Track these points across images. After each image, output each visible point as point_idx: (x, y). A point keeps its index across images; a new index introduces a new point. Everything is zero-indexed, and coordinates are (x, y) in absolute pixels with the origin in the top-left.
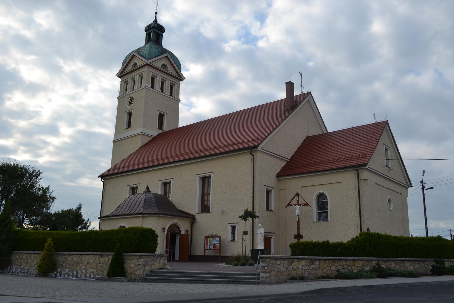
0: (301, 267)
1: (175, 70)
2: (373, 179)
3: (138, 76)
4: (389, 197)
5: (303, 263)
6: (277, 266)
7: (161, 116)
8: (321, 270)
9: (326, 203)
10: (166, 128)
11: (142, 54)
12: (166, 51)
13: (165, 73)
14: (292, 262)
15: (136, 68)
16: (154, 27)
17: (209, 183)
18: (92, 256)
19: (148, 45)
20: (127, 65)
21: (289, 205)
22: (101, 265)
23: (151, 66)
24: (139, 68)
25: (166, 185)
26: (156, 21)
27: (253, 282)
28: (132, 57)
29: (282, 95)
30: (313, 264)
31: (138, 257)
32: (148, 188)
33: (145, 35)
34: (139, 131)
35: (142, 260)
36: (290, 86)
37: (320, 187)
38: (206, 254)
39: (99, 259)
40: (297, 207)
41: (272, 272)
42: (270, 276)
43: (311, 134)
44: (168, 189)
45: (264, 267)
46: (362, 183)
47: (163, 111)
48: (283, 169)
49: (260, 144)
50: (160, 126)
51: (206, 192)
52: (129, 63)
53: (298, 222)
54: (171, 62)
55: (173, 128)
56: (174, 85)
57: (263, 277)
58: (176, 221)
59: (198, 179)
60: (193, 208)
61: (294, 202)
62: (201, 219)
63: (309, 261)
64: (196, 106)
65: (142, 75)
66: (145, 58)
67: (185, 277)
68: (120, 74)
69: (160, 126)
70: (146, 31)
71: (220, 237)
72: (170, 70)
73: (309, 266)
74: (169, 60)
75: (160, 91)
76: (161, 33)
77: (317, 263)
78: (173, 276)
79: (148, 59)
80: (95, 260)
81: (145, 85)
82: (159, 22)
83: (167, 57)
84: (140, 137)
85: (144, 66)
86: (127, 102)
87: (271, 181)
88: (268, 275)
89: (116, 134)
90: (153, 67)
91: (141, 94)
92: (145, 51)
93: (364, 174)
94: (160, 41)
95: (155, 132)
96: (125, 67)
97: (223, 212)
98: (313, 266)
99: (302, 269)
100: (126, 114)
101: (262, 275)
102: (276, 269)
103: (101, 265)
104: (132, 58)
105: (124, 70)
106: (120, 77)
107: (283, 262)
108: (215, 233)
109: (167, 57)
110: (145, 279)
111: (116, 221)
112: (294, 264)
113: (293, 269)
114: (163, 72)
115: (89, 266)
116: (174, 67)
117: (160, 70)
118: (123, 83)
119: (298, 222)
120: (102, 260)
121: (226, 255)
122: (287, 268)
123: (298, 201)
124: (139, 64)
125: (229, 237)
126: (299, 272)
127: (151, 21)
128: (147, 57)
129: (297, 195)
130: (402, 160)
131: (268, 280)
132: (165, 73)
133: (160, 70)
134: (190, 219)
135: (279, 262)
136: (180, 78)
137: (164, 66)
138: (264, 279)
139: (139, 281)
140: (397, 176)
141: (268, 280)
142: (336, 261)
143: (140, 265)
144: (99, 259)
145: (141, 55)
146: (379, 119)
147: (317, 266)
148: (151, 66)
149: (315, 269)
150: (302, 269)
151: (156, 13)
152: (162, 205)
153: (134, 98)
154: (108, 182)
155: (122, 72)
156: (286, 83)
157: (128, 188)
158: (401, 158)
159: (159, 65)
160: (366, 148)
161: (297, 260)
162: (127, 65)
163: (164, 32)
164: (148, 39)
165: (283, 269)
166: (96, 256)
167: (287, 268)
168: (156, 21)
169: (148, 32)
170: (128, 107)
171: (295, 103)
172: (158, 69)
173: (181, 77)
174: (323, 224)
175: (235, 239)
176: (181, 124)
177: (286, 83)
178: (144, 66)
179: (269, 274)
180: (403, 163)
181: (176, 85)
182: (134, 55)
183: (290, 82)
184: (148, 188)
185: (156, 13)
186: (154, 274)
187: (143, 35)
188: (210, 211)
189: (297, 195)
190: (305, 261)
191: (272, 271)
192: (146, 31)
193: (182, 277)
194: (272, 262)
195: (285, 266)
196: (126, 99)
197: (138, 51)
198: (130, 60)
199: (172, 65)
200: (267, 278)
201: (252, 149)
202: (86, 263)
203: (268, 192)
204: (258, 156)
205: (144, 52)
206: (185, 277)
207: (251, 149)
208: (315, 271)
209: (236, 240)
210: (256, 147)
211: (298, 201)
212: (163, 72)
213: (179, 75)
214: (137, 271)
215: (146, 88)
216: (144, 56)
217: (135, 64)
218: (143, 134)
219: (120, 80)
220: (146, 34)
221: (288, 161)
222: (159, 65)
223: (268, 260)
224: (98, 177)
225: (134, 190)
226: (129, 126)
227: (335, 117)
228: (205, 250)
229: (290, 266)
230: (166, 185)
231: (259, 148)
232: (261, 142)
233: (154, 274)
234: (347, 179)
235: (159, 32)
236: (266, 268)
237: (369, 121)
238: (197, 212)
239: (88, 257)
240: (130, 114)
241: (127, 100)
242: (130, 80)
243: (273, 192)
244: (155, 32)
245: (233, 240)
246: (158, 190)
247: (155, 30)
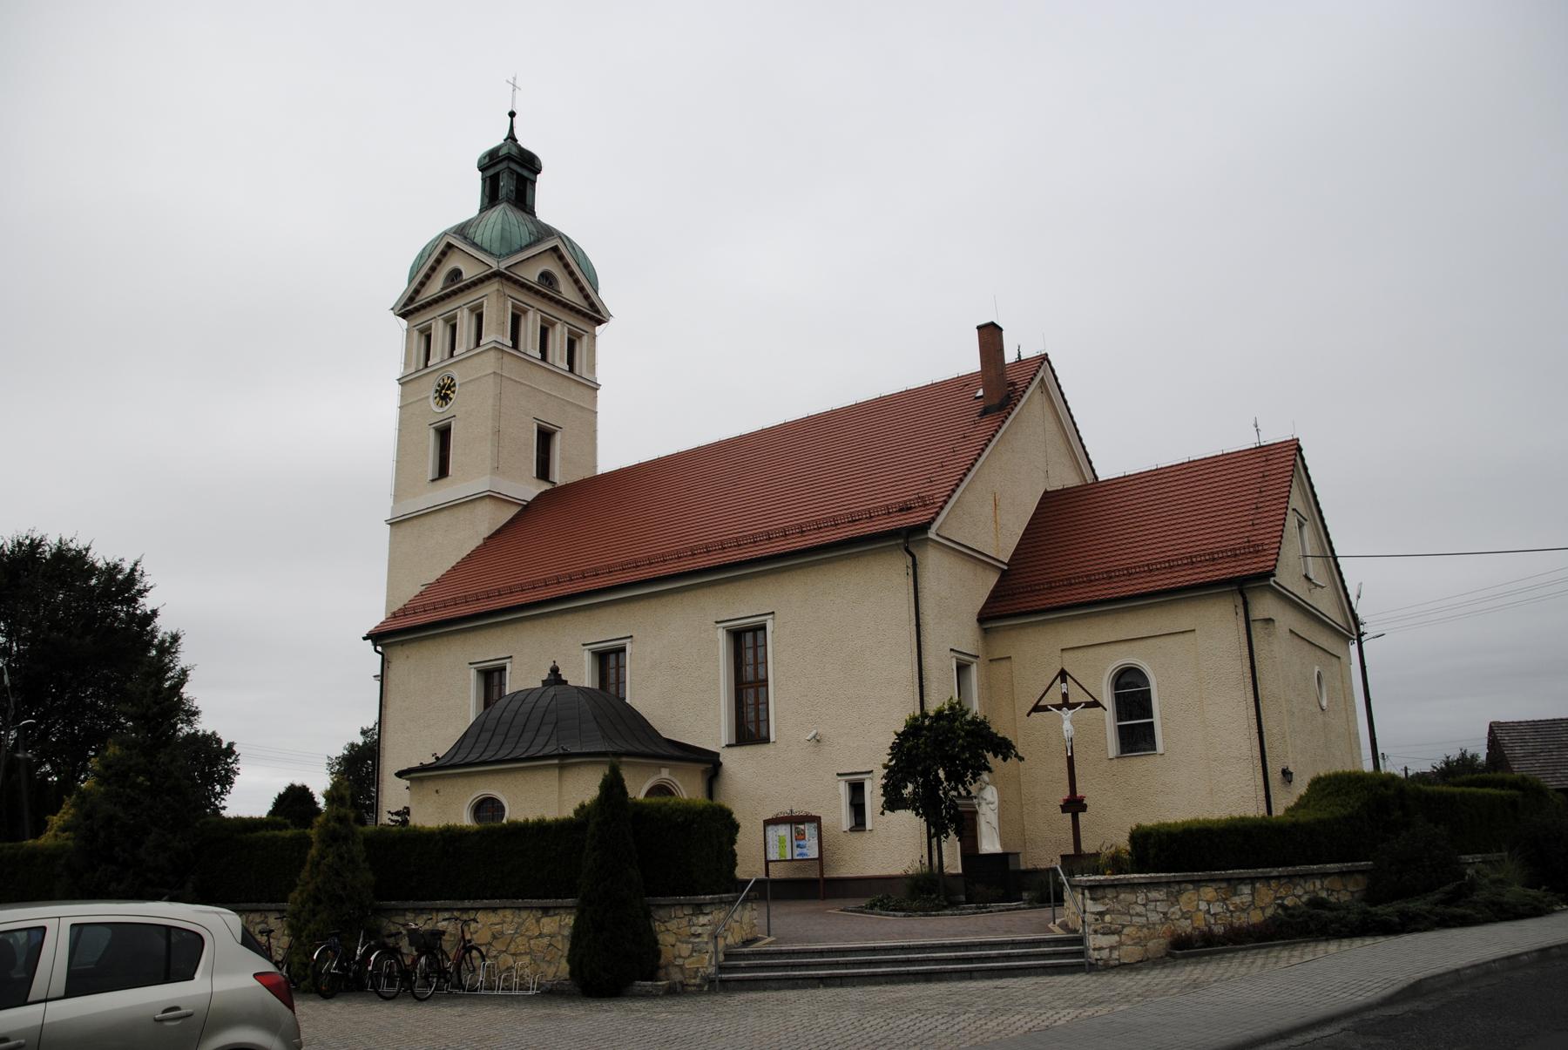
0: (1203, 906)
1: (582, 289)
2: (1286, 619)
3: (466, 312)
4: (1317, 669)
5: (1209, 892)
6: (1139, 909)
7: (545, 437)
8: (1259, 912)
9: (1147, 695)
10: (560, 475)
11: (478, 240)
12: (547, 232)
13: (551, 299)
14: (1180, 893)
15: (457, 286)
16: (509, 157)
17: (620, 667)
18: (508, 913)
19: (496, 214)
20: (428, 276)
21: (1037, 708)
22: (546, 940)
23: (509, 279)
24: (468, 287)
25: (608, 659)
26: (511, 137)
27: (1072, 965)
28: (446, 248)
29: (971, 362)
30: (1235, 894)
31: (688, 911)
32: (555, 670)
33: (480, 182)
34: (480, 485)
35: (703, 920)
36: (990, 335)
37: (1124, 647)
38: (772, 876)
39: (538, 921)
40: (1067, 714)
41: (1126, 931)
42: (1121, 944)
43: (1056, 485)
44: (613, 671)
45: (1102, 914)
46: (1257, 629)
47: (551, 419)
48: (994, 597)
49: (934, 519)
50: (543, 472)
51: (749, 673)
52: (433, 269)
53: (1070, 760)
54: (567, 266)
55: (588, 475)
56: (580, 337)
57: (1100, 949)
58: (665, 774)
59: (721, 637)
60: (708, 725)
61: (1054, 697)
62: (739, 765)
63: (1224, 885)
64: (649, 402)
65: (481, 305)
66: (491, 254)
67: (846, 965)
68: (405, 305)
69: (543, 472)
70: (482, 169)
71: (816, 820)
72: (567, 291)
73: (1224, 900)
74: (561, 257)
75: (539, 356)
76: (531, 176)
77: (1246, 890)
78: (807, 966)
79: (499, 257)
80: (520, 925)
81: (493, 338)
82: (525, 142)
83: (555, 249)
84: (486, 508)
85: (488, 278)
86: (432, 394)
87: (966, 636)
88: (1114, 939)
89: (398, 496)
90: (516, 282)
91: (477, 376)
92: (487, 234)
93: (1264, 606)
94: (528, 202)
95: (528, 489)
96: (422, 284)
97: (817, 740)
98: (1237, 900)
99: (1208, 911)
100: (432, 433)
101: (1093, 941)
102: (1136, 919)
103: (546, 940)
104: (444, 254)
105: (417, 292)
106: (404, 316)
107: (1154, 895)
108: (800, 809)
109: (555, 249)
110: (722, 981)
111: (461, 782)
112: (1184, 898)
113: (1185, 916)
114: (544, 296)
115: (498, 945)
116: (577, 281)
117: (537, 292)
118: (416, 333)
119: (1070, 760)
120: (549, 924)
121: (835, 875)
122: (1165, 914)
123: (1065, 696)
124: (469, 272)
125: (845, 818)
126: (1200, 923)
127: (496, 139)
128: (496, 248)
129: (1063, 675)
130: (1335, 558)
131: (1115, 954)
132: (551, 299)
133: (537, 292)
134: (702, 767)
135: (1141, 898)
136: (596, 316)
137: (547, 277)
138: (1105, 954)
139: (699, 991)
140: (1324, 603)
141: (1115, 954)
142: (1297, 880)
143: (699, 935)
144: (538, 921)
145: (474, 245)
146: (1271, 436)
147: (1247, 899)
148: (509, 279)
149: (1243, 910)
150: (1208, 911)
151: (512, 114)
152: (601, 721)
153: (457, 382)
154: (390, 652)
155: (411, 299)
156: (979, 328)
157: (473, 673)
158: (1332, 551)
159: (531, 275)
160: (1234, 534)
161: (1190, 887)
162: (428, 276)
163: (537, 171)
164: (491, 196)
165: (1154, 917)
166: (524, 914)
167: (1165, 914)
168: (511, 137)
169: (491, 172)
170: (437, 412)
171: (1005, 387)
172: (448, 296)
173: (598, 312)
174: (1139, 764)
175: (864, 824)
176: (607, 462)
177: (979, 328)
178: (488, 278)
179: (1116, 938)
180: (1337, 566)
181: (585, 339)
182: (449, 246)
183: (993, 324)
184: (555, 670)
185: (512, 114)
186: (743, 963)
187: (474, 183)
188: (772, 738)
189: (1063, 675)
190: (1215, 886)
191: (1124, 926)
192: (482, 168)
193: (837, 965)
194: (1122, 896)
195: (1161, 907)
196: (431, 385)
197: (462, 230)
198: (438, 261)
199: (571, 273)
200: (1112, 948)
201: (907, 537)
202: (489, 939)
203: (962, 668)
204: (934, 563)
205: (482, 235)
206: (846, 965)
207: (907, 537)
208: (1244, 916)
209: (869, 826)
210: (925, 527)
211: (1065, 696)
212: (544, 296)
213: (592, 305)
214: (690, 956)
215: (498, 349)
216: (486, 246)
217: (456, 274)
218: (492, 497)
219: (404, 323)
220: (484, 180)
221: (1003, 571)
222: (531, 275)
223: (1110, 893)
224: (175, 638)
225: (491, 677)
226: (443, 471)
227: (1130, 427)
228: (767, 862)
229: (1173, 905)
230: (608, 659)
231: (931, 534)
232: (938, 514)
233: (743, 963)
234: (1213, 630)
235: (526, 173)
236: (1108, 918)
237: (1243, 440)
238: (724, 742)
239: (493, 918)
240: (444, 434)
241: (429, 387)
242: (441, 323)
243: (974, 668)
244: (512, 171)
245: (859, 822)
246: (582, 674)
247: (513, 166)
